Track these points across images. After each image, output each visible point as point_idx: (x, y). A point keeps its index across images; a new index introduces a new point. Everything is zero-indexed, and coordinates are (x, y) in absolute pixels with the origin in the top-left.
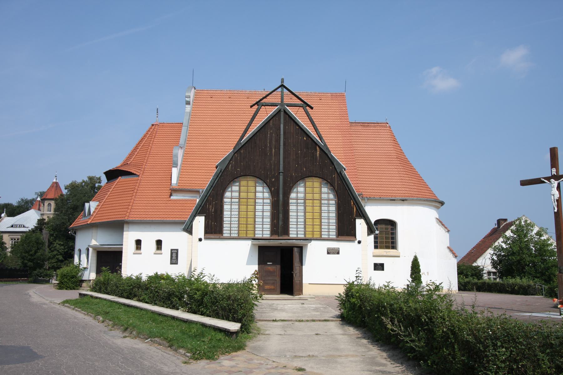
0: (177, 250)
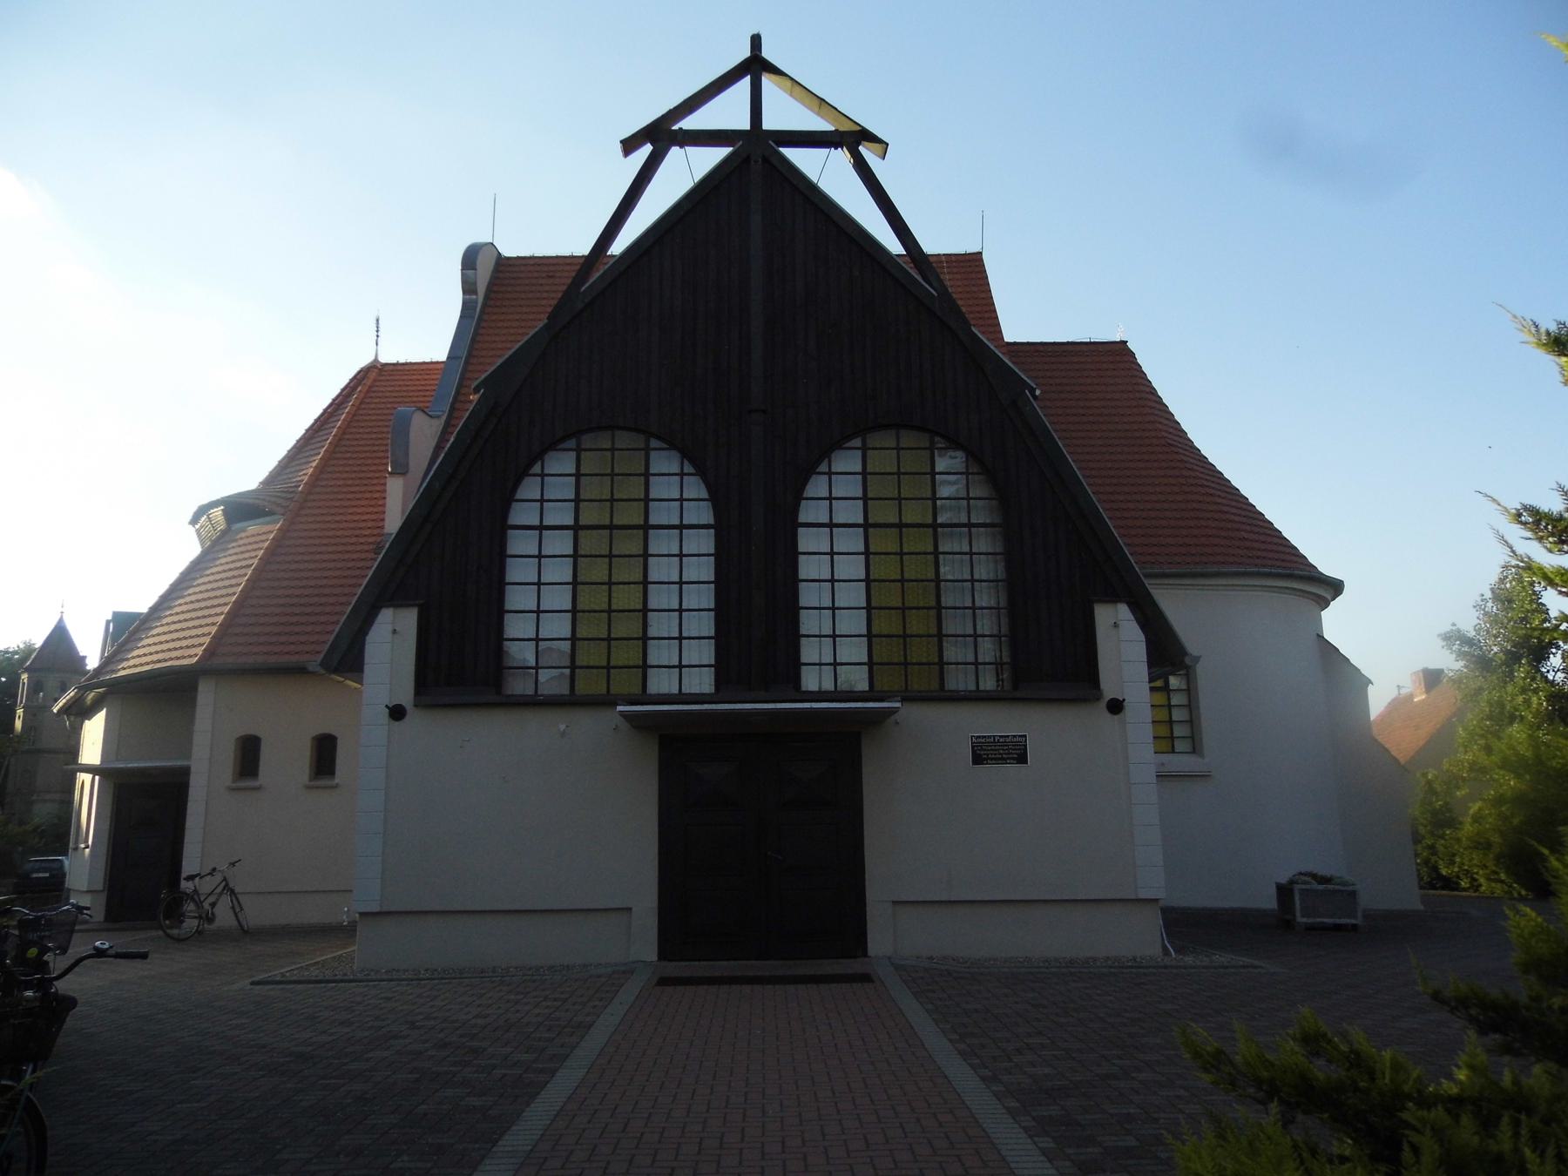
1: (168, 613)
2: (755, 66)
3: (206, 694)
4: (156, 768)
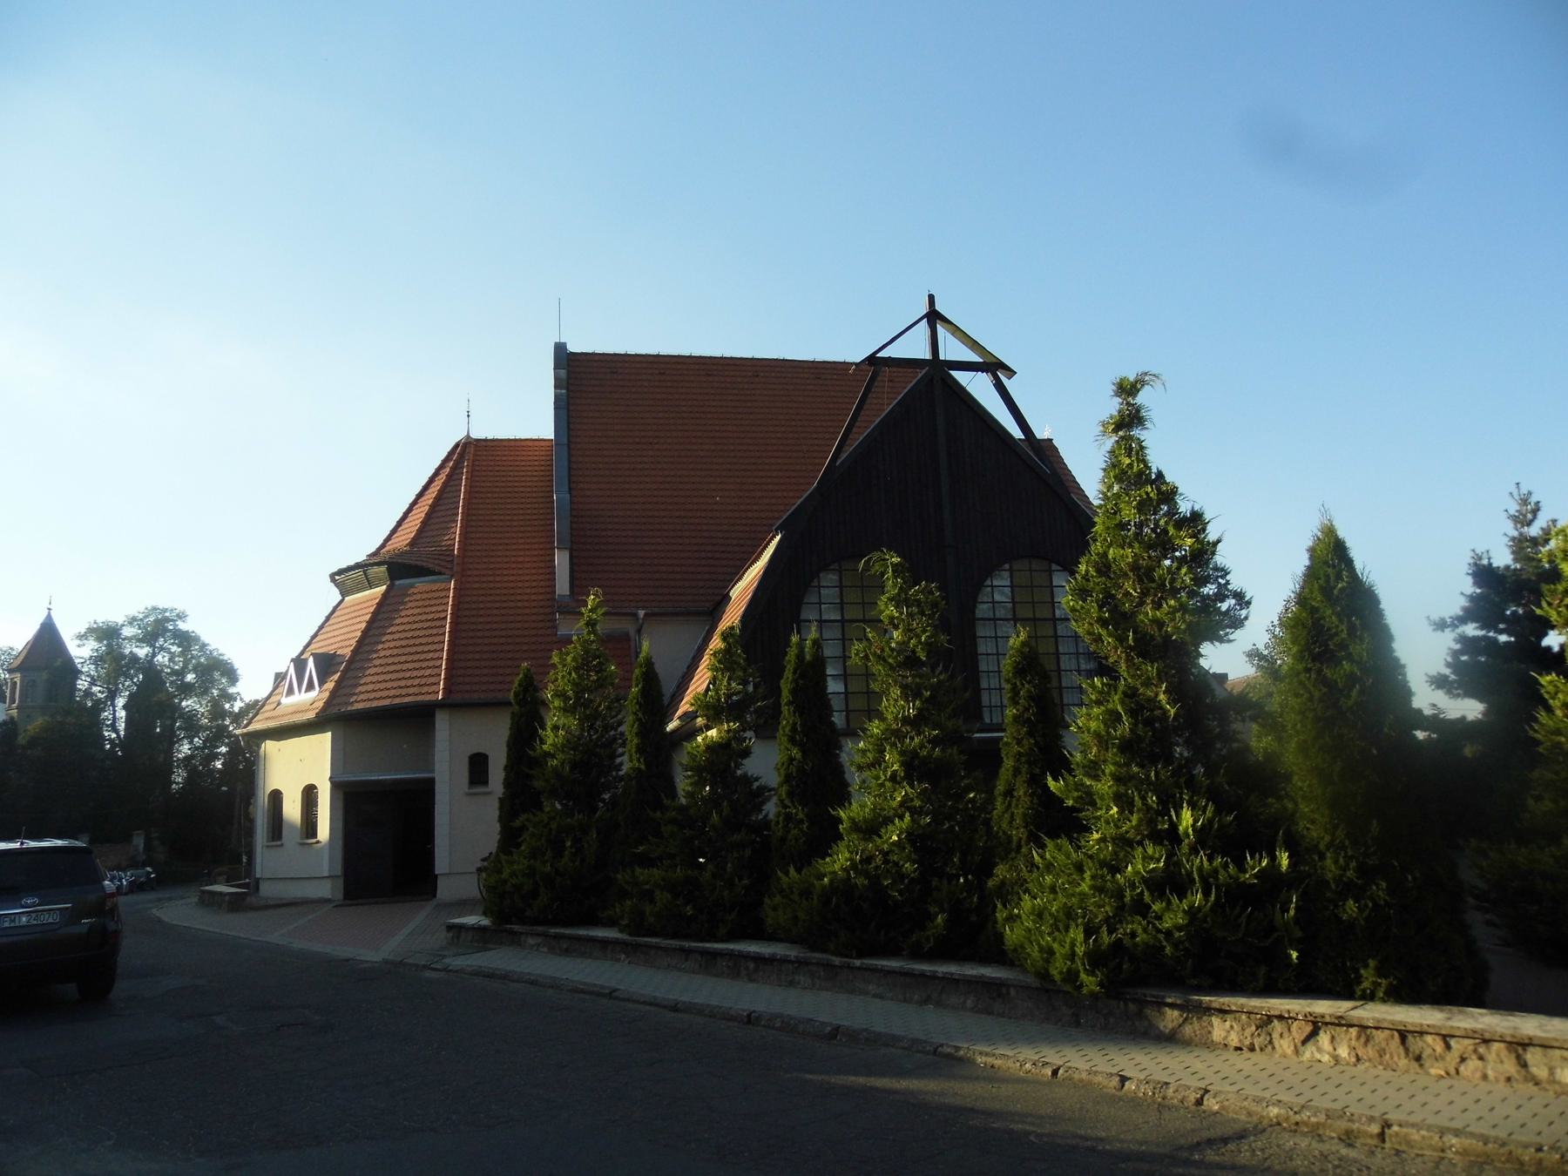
1: (375, 656)
2: (934, 317)
3: (442, 722)
4: (391, 779)
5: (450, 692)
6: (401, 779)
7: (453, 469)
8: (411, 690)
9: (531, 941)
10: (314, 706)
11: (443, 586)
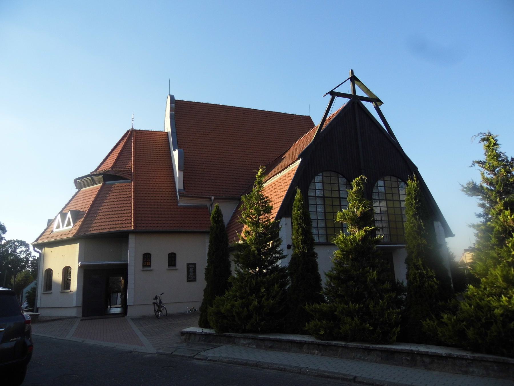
0: (195, 264)
2: (353, 79)
3: (132, 239)
4: (108, 264)
5: (136, 226)
6: (115, 264)
7: (128, 140)
8: (118, 226)
9: (243, 342)
10: (72, 232)
11: (128, 184)
